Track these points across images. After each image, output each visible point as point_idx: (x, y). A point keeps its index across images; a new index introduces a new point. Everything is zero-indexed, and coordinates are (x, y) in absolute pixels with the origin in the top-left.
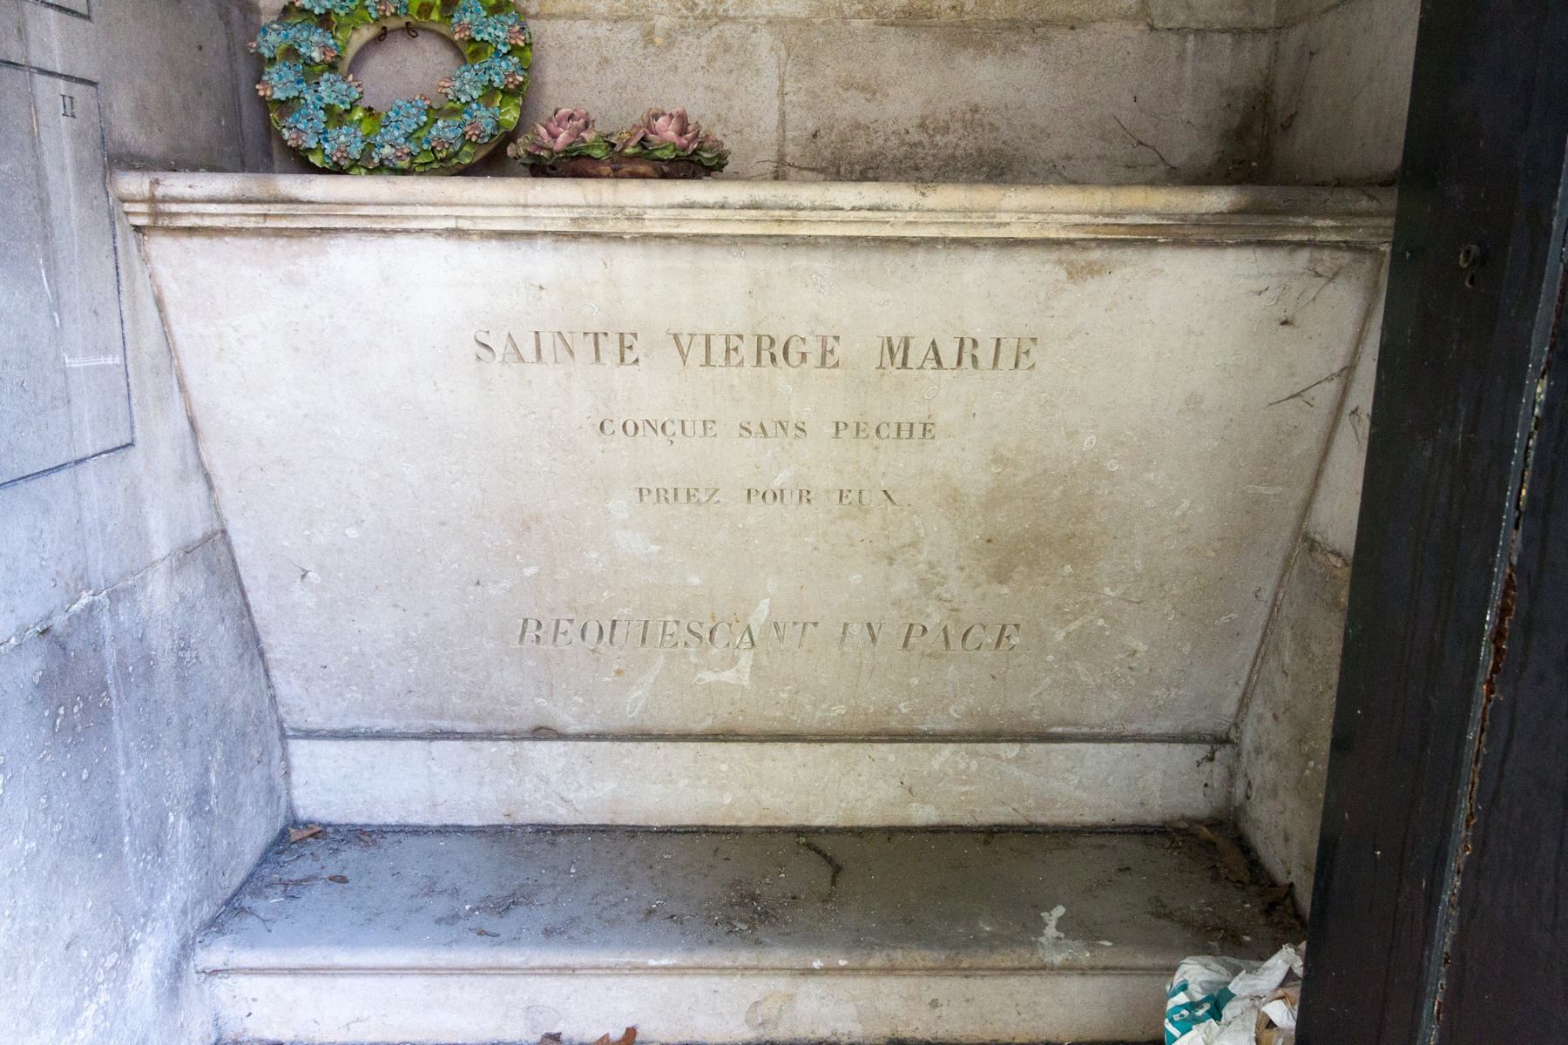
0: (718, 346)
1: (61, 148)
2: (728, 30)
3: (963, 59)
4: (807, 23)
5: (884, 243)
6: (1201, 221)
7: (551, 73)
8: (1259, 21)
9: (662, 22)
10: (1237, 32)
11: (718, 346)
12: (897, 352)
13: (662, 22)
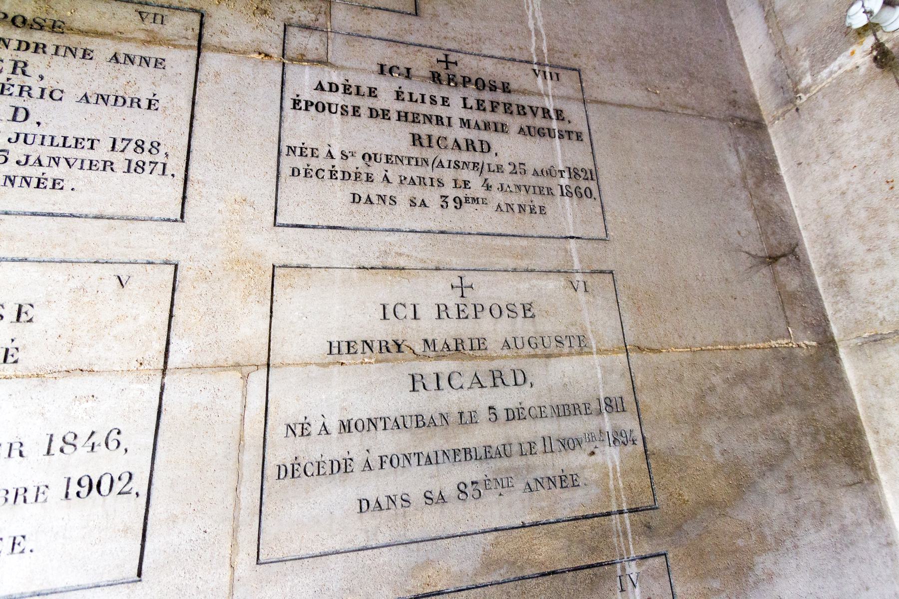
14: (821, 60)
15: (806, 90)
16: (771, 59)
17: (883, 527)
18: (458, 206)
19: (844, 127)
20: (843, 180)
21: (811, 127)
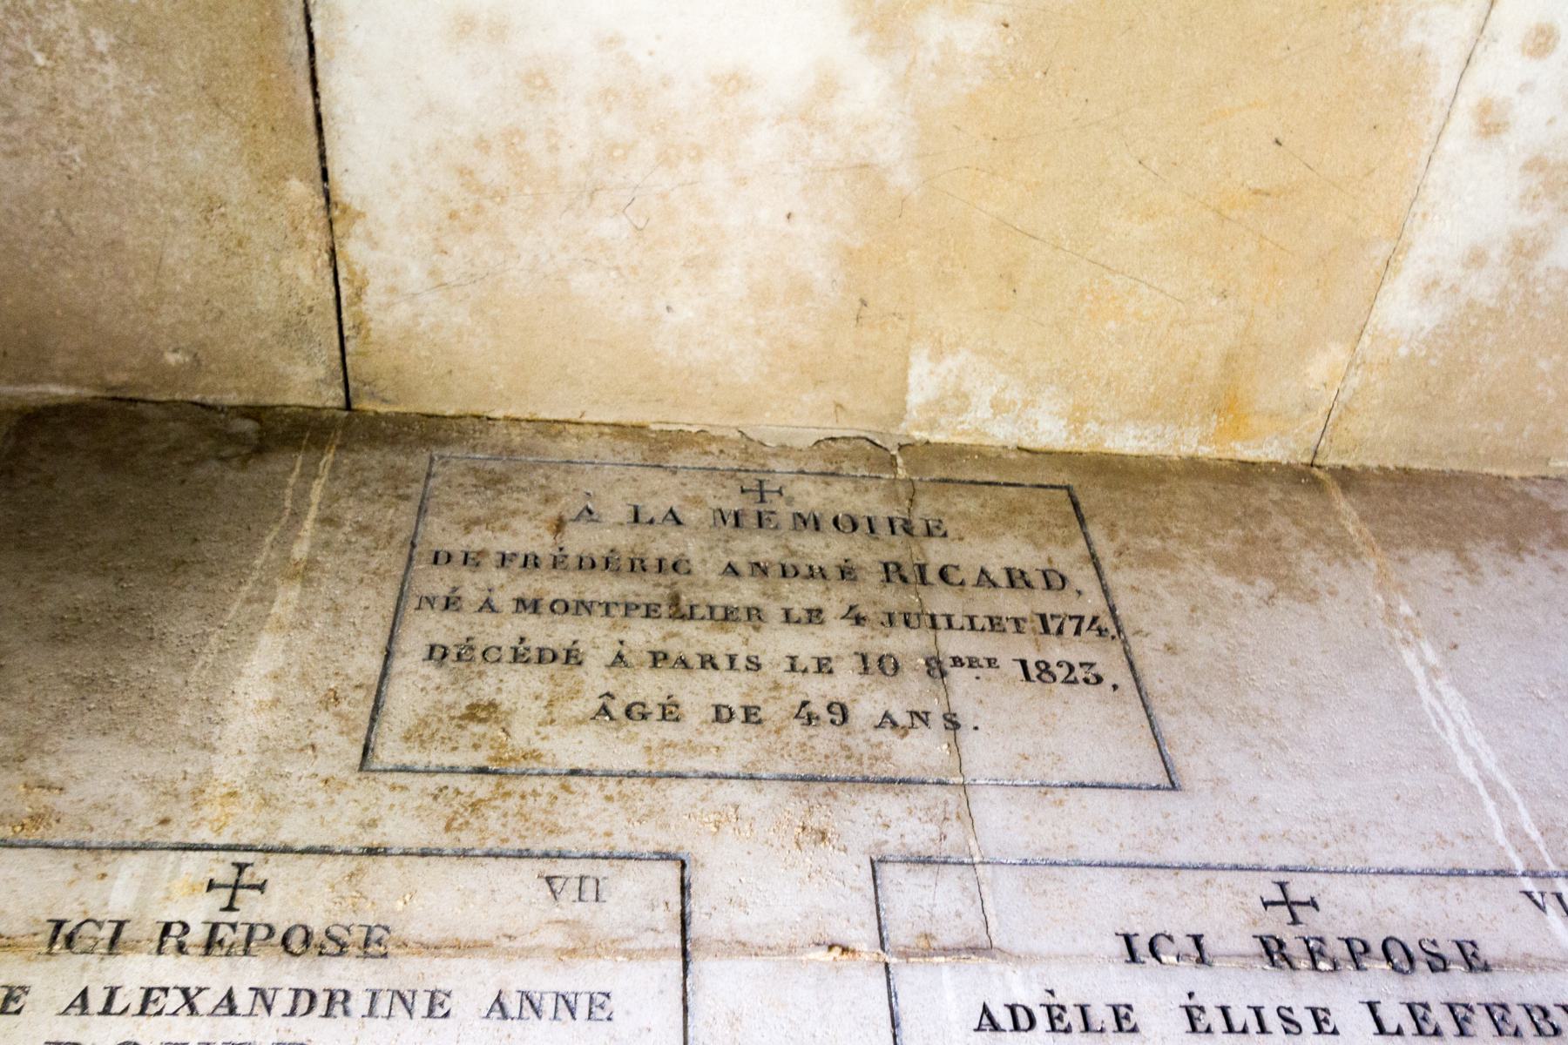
17: (498, 434)
18: (839, 719)
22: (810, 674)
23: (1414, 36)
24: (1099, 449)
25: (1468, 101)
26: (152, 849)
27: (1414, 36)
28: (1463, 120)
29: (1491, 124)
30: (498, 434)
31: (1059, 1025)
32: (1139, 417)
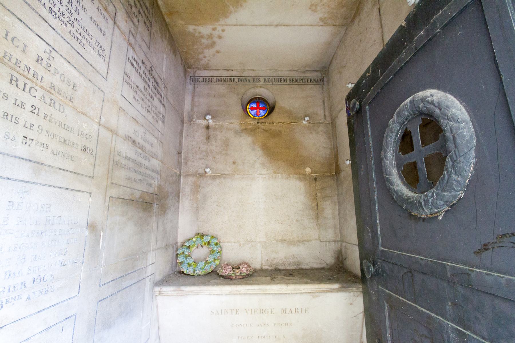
0: (253, 311)
1: (148, 284)
2: (253, 243)
3: (291, 247)
4: (266, 242)
5: (281, 294)
6: (334, 289)
7: (224, 251)
8: (338, 239)
9: (242, 243)
10: (335, 241)
11: (253, 311)
12: (284, 311)
13: (242, 243)
14: (198, 118)
15: (194, 122)
16: (190, 109)
17: (177, 204)
18: (40, 131)
19: (197, 133)
20: (194, 143)
21: (192, 129)
22: (28, 129)
23: (221, 19)
24: (349, 91)
25: (216, 26)
26: (337, 157)
27: (221, 19)
28: (213, 27)
29: (214, 29)
30: (177, 204)
31: (23, 107)
32: (164, 3)
